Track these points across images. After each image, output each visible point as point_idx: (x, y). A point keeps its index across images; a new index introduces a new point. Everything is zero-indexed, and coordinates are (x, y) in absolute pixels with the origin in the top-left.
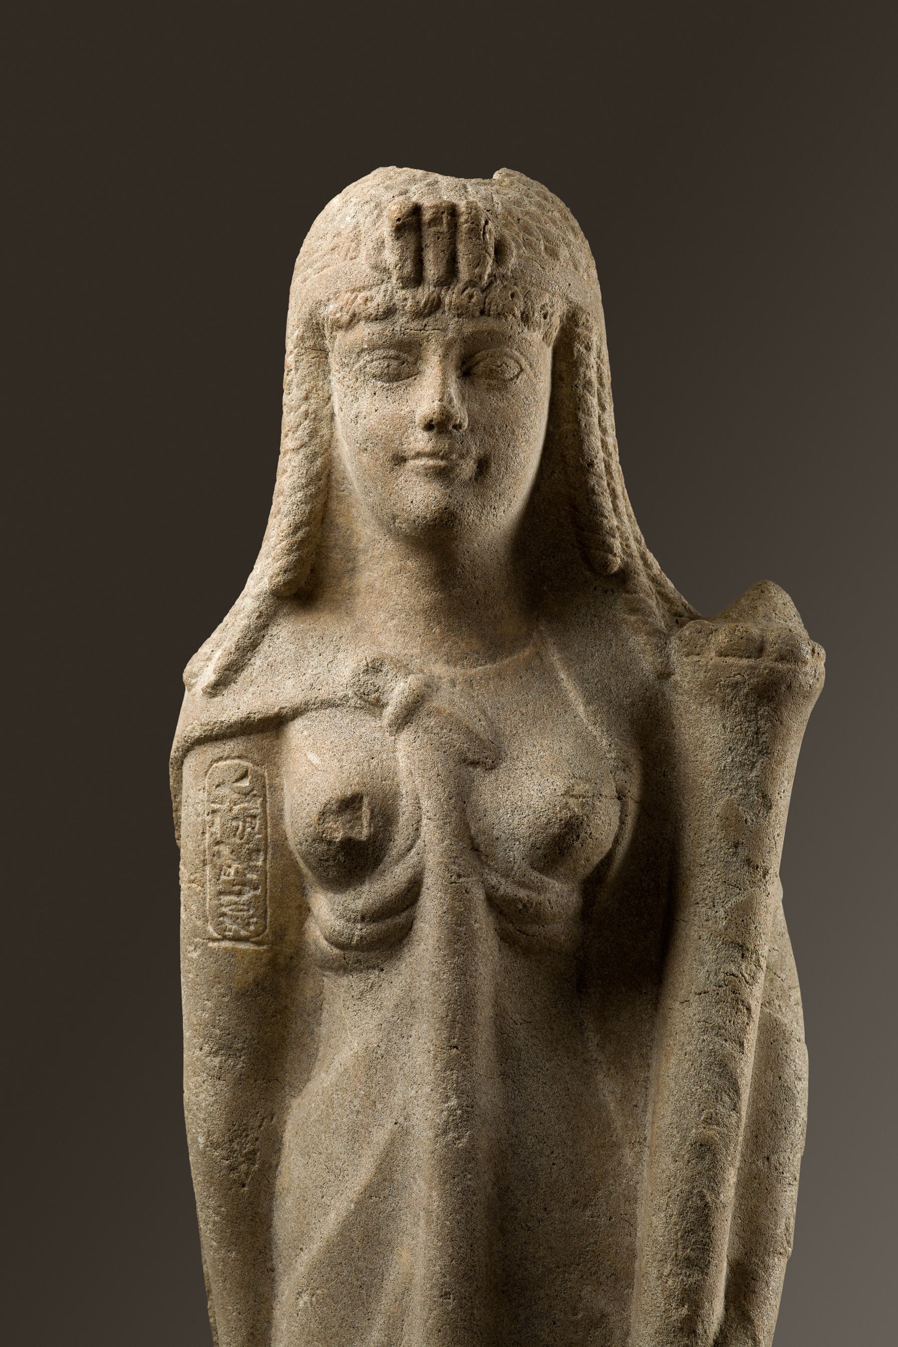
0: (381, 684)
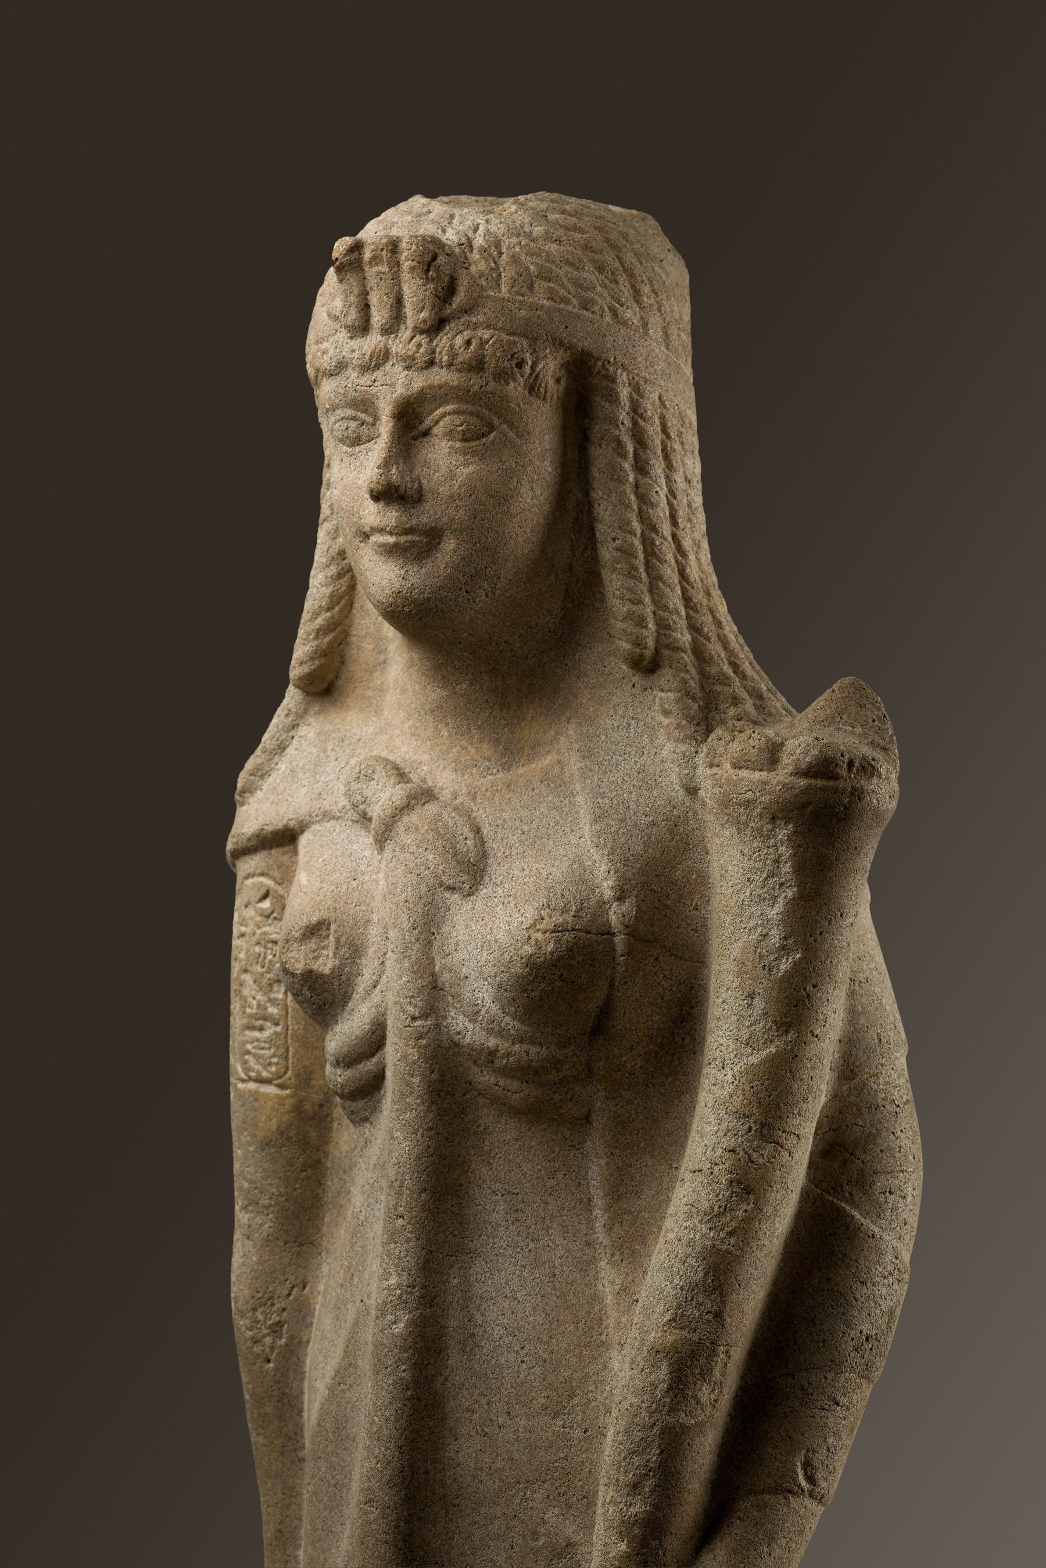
0: (369, 794)
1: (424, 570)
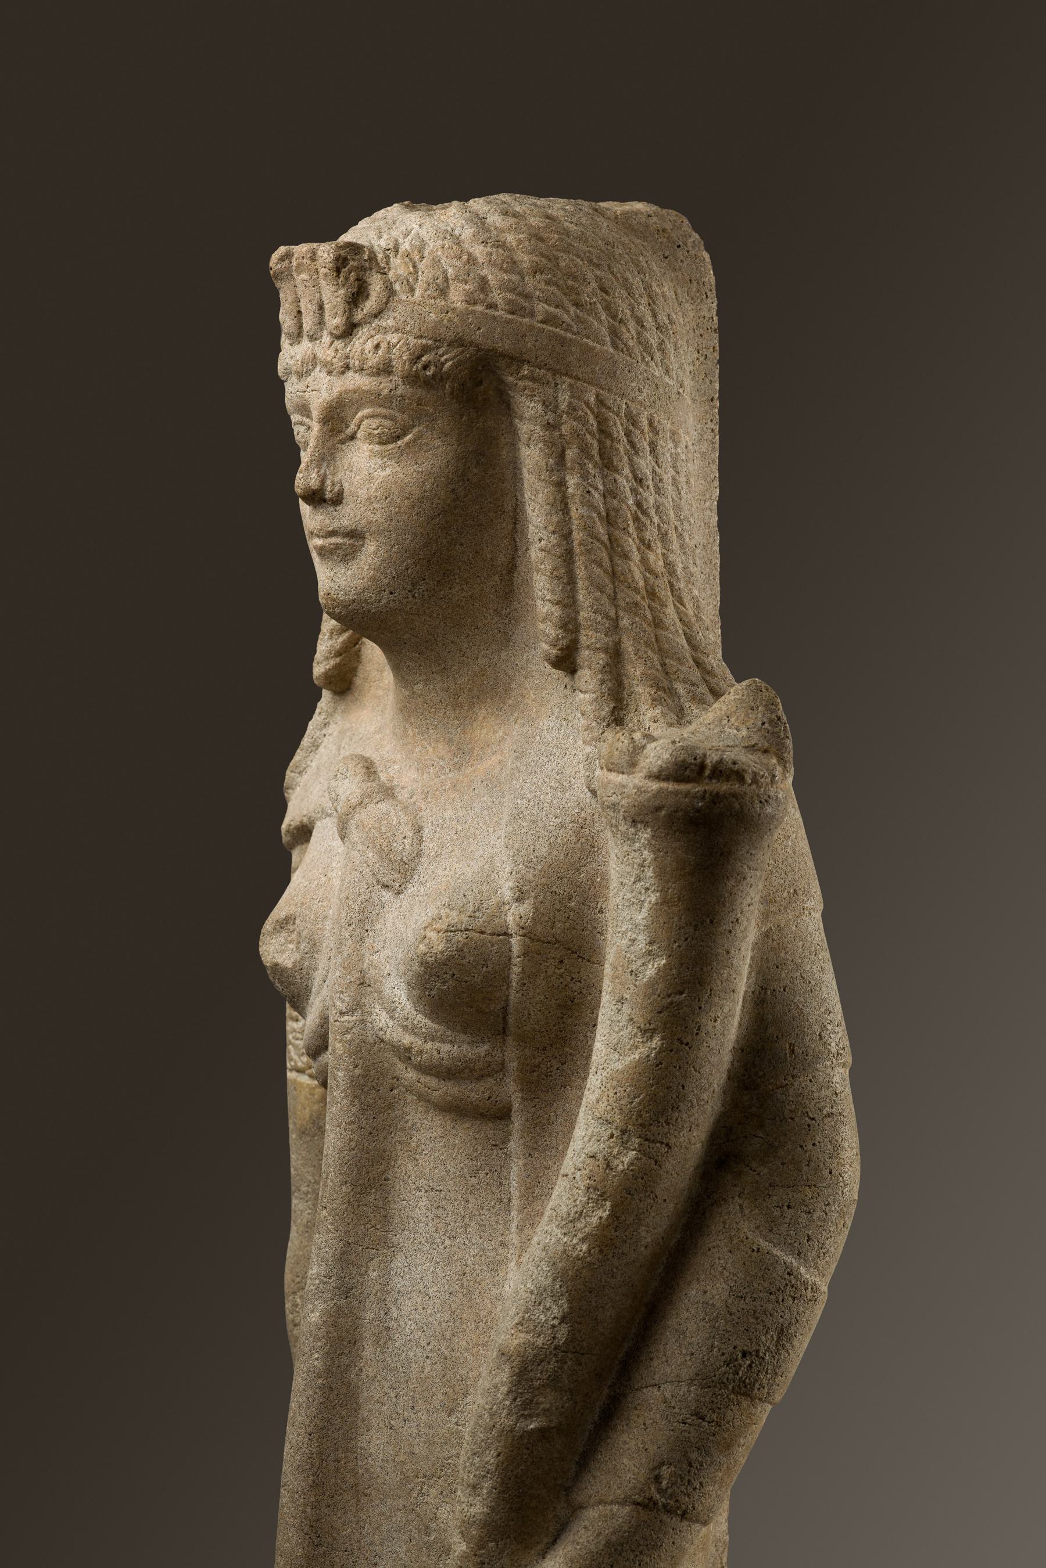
1: (350, 572)
